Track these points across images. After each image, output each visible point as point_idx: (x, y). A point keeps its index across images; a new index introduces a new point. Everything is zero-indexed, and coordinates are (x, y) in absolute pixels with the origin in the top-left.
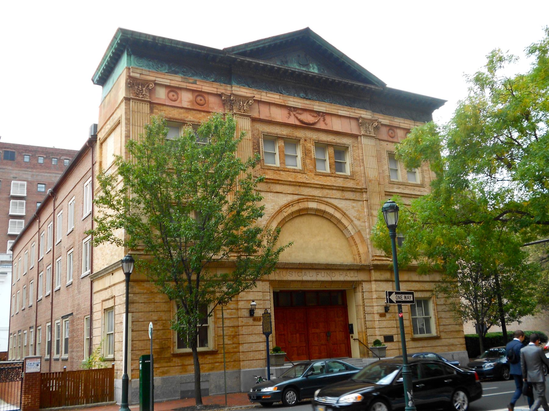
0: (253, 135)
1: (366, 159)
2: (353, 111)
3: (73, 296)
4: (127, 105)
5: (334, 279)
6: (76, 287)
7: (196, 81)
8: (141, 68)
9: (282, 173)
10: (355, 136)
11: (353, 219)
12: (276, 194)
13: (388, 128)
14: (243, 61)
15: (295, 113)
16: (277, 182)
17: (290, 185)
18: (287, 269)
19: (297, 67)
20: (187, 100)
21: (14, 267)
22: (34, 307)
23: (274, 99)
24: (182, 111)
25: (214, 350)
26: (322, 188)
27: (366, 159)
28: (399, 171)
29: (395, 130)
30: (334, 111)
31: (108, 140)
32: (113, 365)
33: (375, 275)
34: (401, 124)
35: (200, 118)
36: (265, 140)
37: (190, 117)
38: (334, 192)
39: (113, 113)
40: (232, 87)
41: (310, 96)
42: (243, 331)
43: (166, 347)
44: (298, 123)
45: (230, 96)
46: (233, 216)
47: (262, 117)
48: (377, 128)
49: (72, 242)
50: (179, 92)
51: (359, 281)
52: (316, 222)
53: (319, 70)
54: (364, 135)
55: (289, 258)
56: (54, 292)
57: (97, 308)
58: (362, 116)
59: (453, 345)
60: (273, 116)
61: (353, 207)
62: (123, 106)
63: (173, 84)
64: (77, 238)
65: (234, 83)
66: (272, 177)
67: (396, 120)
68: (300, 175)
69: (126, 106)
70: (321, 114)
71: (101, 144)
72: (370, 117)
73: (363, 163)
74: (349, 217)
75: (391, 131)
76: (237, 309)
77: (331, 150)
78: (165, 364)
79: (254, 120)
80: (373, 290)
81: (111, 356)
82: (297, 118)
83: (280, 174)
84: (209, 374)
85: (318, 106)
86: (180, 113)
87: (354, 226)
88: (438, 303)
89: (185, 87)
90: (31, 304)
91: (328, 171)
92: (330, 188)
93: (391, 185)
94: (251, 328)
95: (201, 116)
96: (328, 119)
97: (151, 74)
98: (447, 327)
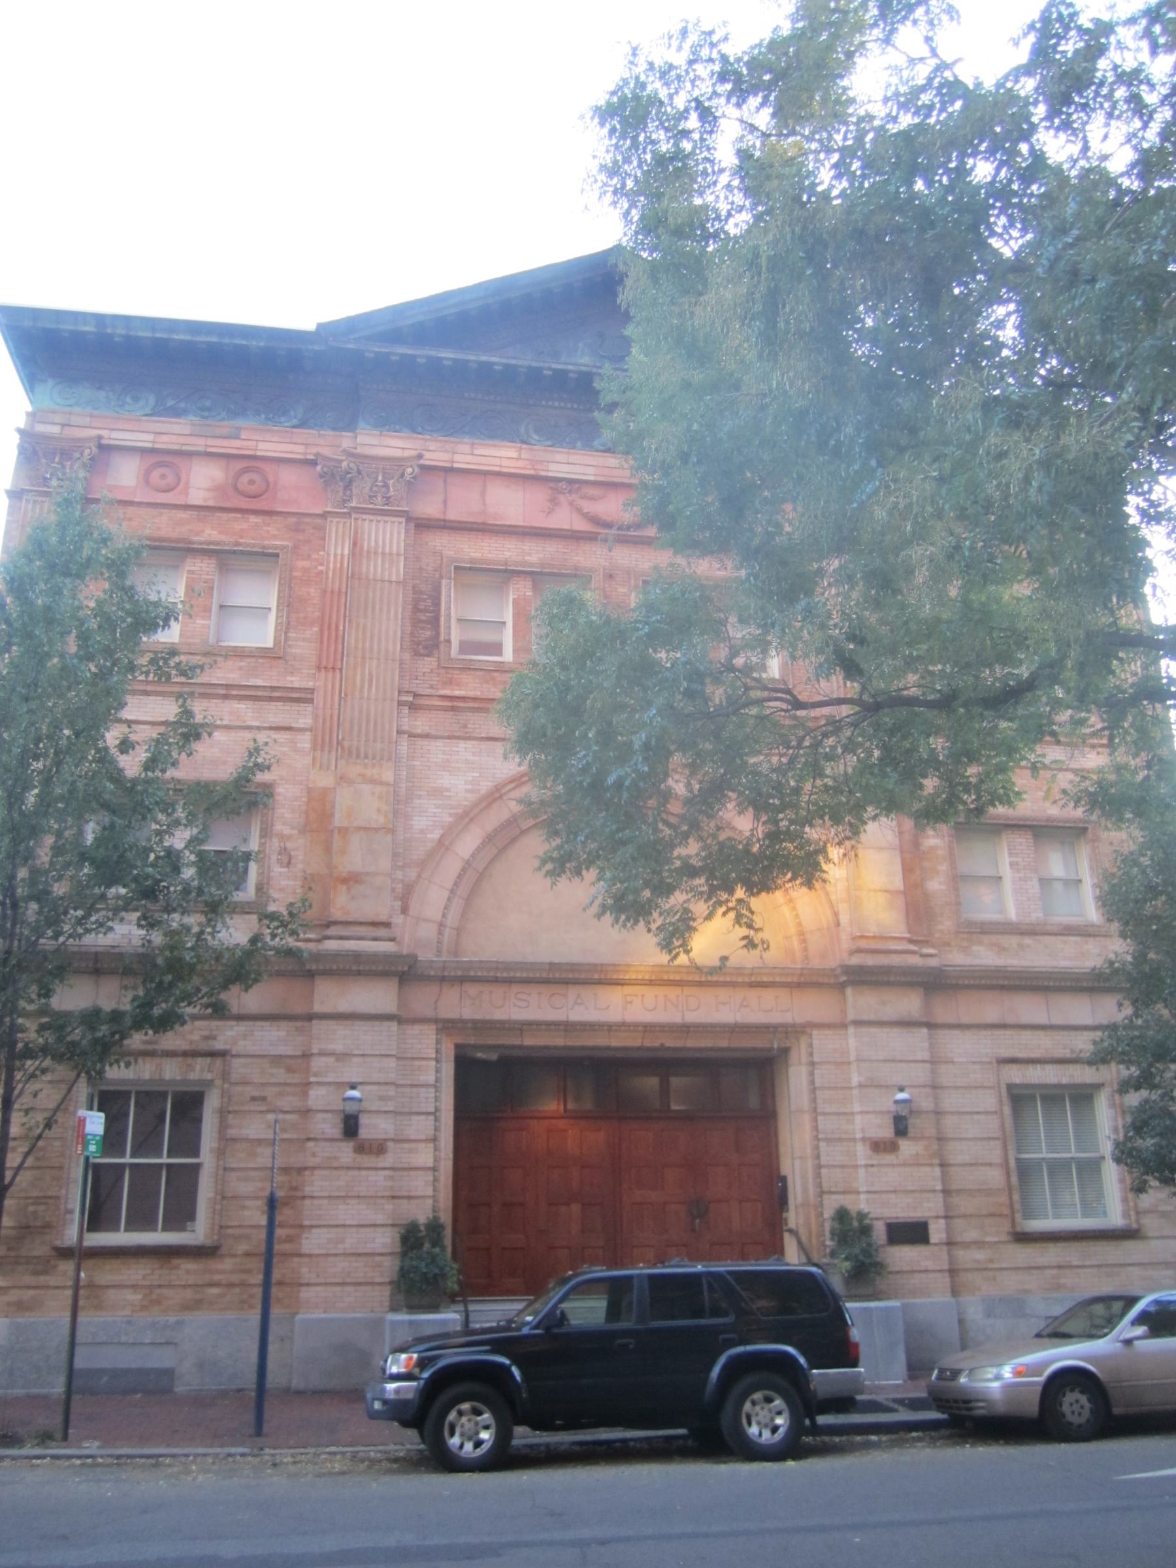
7: (239, 429)
12: (484, 745)
14: (435, 364)
18: (510, 981)
33: (862, 1003)
42: (316, 1184)
43: (38, 1224)
44: (581, 525)
46: (1168, 1021)
47: (452, 515)
63: (164, 442)
70: (563, 485)
76: (306, 1112)
78: (28, 1279)
80: (852, 1057)
82: (579, 511)
84: (179, 1323)
89: (201, 449)
95: (245, 526)
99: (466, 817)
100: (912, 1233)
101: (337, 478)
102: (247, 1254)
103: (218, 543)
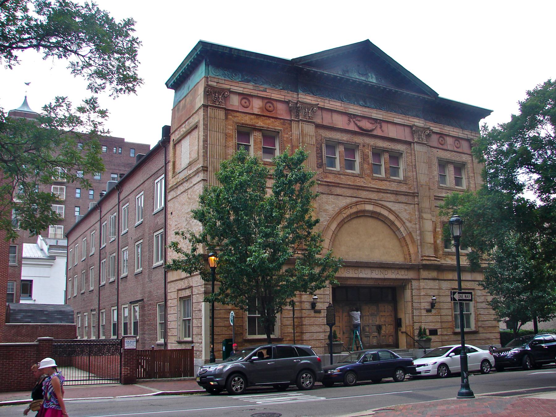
0: (317, 140)
1: (420, 165)
2: (407, 119)
3: (143, 284)
4: (205, 111)
5: (386, 277)
6: (147, 276)
7: (266, 89)
8: (217, 77)
9: (342, 177)
10: (409, 143)
11: (405, 221)
12: (336, 197)
13: (438, 136)
15: (354, 120)
16: (337, 185)
17: (349, 188)
19: (357, 77)
20: (258, 106)
21: (69, 253)
22: (96, 292)
23: (336, 107)
24: (253, 117)
25: (280, 337)
26: (378, 192)
27: (420, 165)
28: (448, 177)
29: (445, 137)
30: (390, 119)
31: (183, 142)
32: (193, 347)
33: (424, 274)
34: (450, 132)
35: (269, 124)
36: (327, 146)
37: (260, 123)
38: (389, 195)
39: (190, 118)
40: (298, 95)
41: (368, 104)
42: (306, 321)
44: (357, 129)
45: (297, 104)
47: (325, 124)
48: (428, 136)
49: (140, 234)
50: (251, 99)
51: (408, 279)
52: (372, 223)
53: (377, 79)
54: (417, 142)
55: (347, 257)
56: (119, 280)
57: (172, 296)
58: (416, 124)
59: (489, 339)
60: (334, 122)
61: (406, 210)
62: (201, 112)
63: (246, 91)
64: (147, 230)
65: (300, 91)
66: (333, 181)
67: (446, 129)
68: (358, 179)
69: (204, 112)
71: (175, 145)
72: (422, 125)
73: (415, 168)
74: (401, 219)
75: (441, 139)
77: (386, 156)
79: (318, 126)
81: (190, 339)
82: (356, 125)
83: (340, 178)
85: (376, 114)
86: (251, 119)
87: (406, 228)
88: (478, 301)
90: (91, 288)
91: (383, 175)
92: (385, 191)
93: (440, 190)
94: (313, 319)
96: (384, 126)
97: (226, 83)
98: (484, 323)
99: (333, 219)
100: (434, 332)
101: (295, 109)
102: (289, 340)
103: (262, 127)
